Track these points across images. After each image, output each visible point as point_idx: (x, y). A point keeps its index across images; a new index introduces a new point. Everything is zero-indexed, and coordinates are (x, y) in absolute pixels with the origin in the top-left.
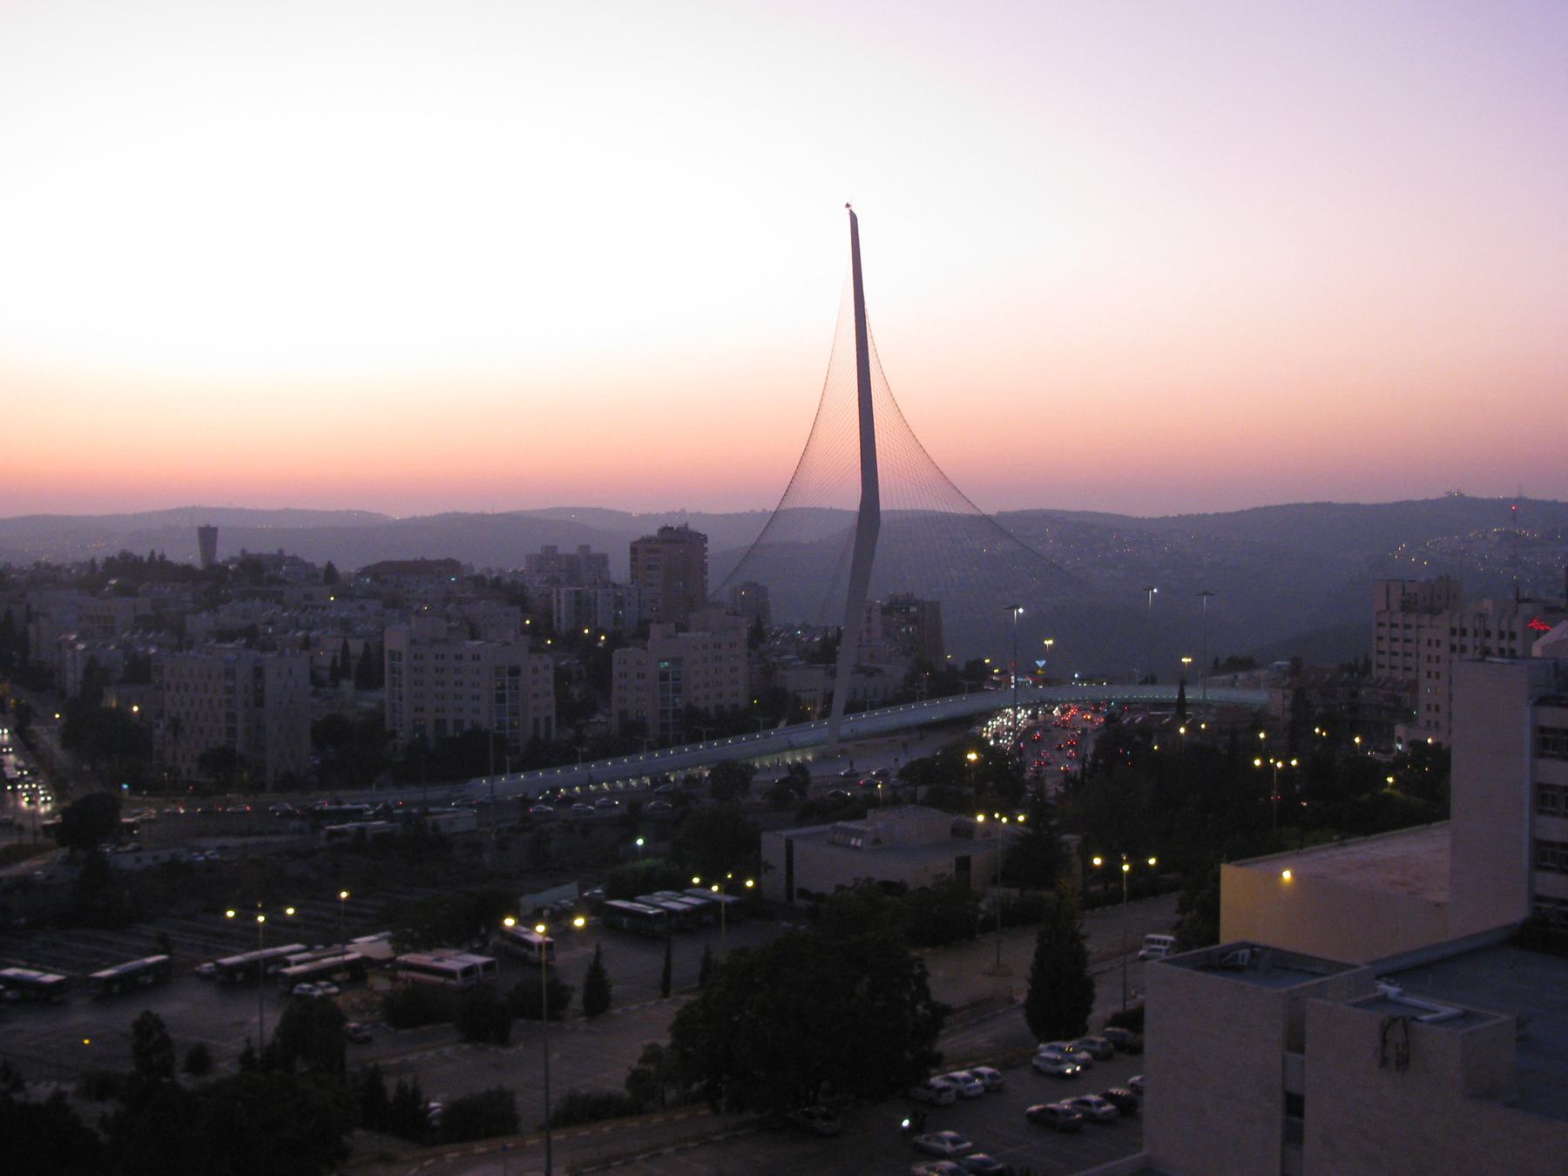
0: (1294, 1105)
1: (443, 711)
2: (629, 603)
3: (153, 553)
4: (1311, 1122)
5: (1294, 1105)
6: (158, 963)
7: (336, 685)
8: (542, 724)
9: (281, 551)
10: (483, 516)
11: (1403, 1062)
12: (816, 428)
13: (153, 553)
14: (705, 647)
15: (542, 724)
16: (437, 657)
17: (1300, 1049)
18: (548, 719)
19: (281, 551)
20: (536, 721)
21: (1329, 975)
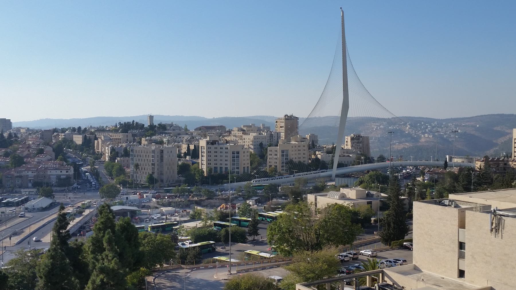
0: (462, 246)
1: (217, 164)
2: (275, 137)
3: (133, 121)
4: (467, 251)
5: (462, 246)
6: (90, 195)
7: (186, 158)
8: (246, 168)
9: (172, 123)
10: (234, 118)
11: (497, 231)
12: (328, 82)
13: (133, 121)
14: (295, 147)
15: (246, 168)
16: (215, 148)
17: (464, 227)
18: (248, 167)
19: (172, 123)
20: (244, 168)
21: (470, 122)
